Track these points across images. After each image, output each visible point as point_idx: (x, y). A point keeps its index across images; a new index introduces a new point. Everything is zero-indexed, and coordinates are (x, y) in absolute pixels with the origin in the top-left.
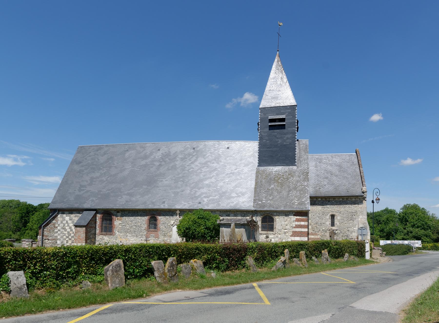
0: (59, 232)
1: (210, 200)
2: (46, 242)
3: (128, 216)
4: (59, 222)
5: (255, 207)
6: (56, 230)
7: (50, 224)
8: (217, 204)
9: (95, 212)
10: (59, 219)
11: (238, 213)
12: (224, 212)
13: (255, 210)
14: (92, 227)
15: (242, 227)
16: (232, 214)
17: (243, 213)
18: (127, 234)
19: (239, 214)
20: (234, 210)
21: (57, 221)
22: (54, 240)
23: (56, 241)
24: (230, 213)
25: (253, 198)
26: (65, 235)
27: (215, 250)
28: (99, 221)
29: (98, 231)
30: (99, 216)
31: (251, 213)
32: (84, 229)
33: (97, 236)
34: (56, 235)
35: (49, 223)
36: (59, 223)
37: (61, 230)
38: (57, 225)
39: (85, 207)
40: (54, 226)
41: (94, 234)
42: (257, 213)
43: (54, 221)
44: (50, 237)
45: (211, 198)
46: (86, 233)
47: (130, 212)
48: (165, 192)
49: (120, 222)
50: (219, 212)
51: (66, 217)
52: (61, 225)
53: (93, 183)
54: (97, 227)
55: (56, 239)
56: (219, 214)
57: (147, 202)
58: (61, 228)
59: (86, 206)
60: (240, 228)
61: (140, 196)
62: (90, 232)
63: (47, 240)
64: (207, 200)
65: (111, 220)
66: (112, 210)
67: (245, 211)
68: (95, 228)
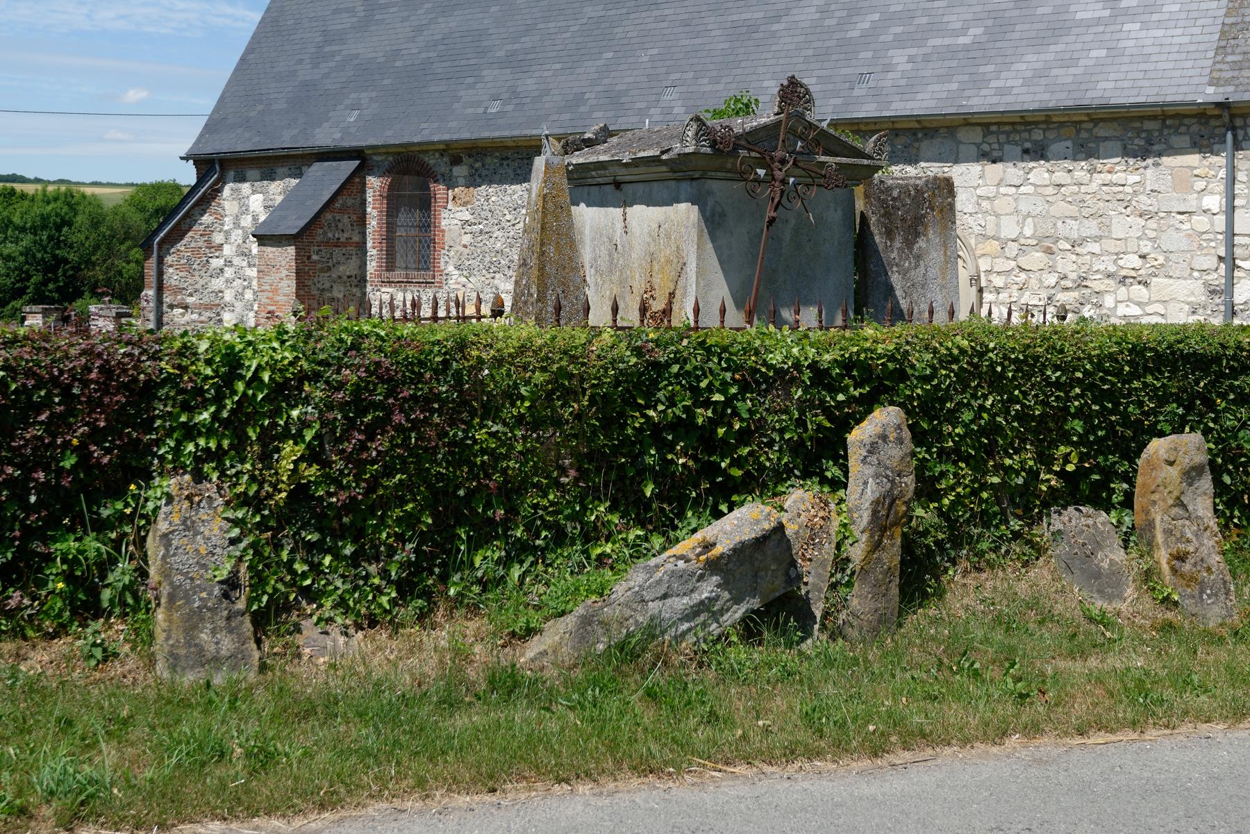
0: (229, 272)
1: (926, 58)
2: (176, 319)
3: (501, 182)
4: (228, 223)
5: (1228, 82)
6: (216, 263)
7: (190, 234)
8: (966, 78)
9: (357, 162)
10: (227, 205)
11: (1101, 131)
12: (1008, 134)
13: (1220, 99)
14: (338, 244)
15: (685, 186)
16: (1059, 139)
17: (1139, 131)
18: (496, 282)
19: (1106, 139)
20: (1067, 109)
21: (220, 217)
22: (208, 307)
23: (218, 314)
24: (1051, 135)
25: (1220, 21)
26: (249, 287)
27: (1010, 374)
28: (375, 213)
29: (374, 264)
30: (375, 185)
31: (1195, 128)
32: (291, 250)
33: (369, 288)
34: (217, 283)
35: (184, 227)
36: (226, 228)
37: (236, 261)
38: (218, 238)
39: (318, 143)
40: (209, 242)
41: (355, 281)
42: (1239, 122)
43: (206, 219)
44: (191, 295)
45: (938, 42)
46: (303, 276)
47: (507, 158)
48: (687, 29)
49: (467, 216)
50: (979, 129)
51: (253, 198)
52: (233, 238)
53: (377, 17)
54: (369, 244)
55: (216, 307)
56: (978, 145)
57: (587, 96)
58: (234, 249)
59: (325, 137)
60: (669, 203)
61: (558, 66)
62: (329, 269)
63: (181, 311)
64: (911, 59)
65: (425, 204)
66: (426, 152)
67: (1154, 118)
68: (362, 247)
